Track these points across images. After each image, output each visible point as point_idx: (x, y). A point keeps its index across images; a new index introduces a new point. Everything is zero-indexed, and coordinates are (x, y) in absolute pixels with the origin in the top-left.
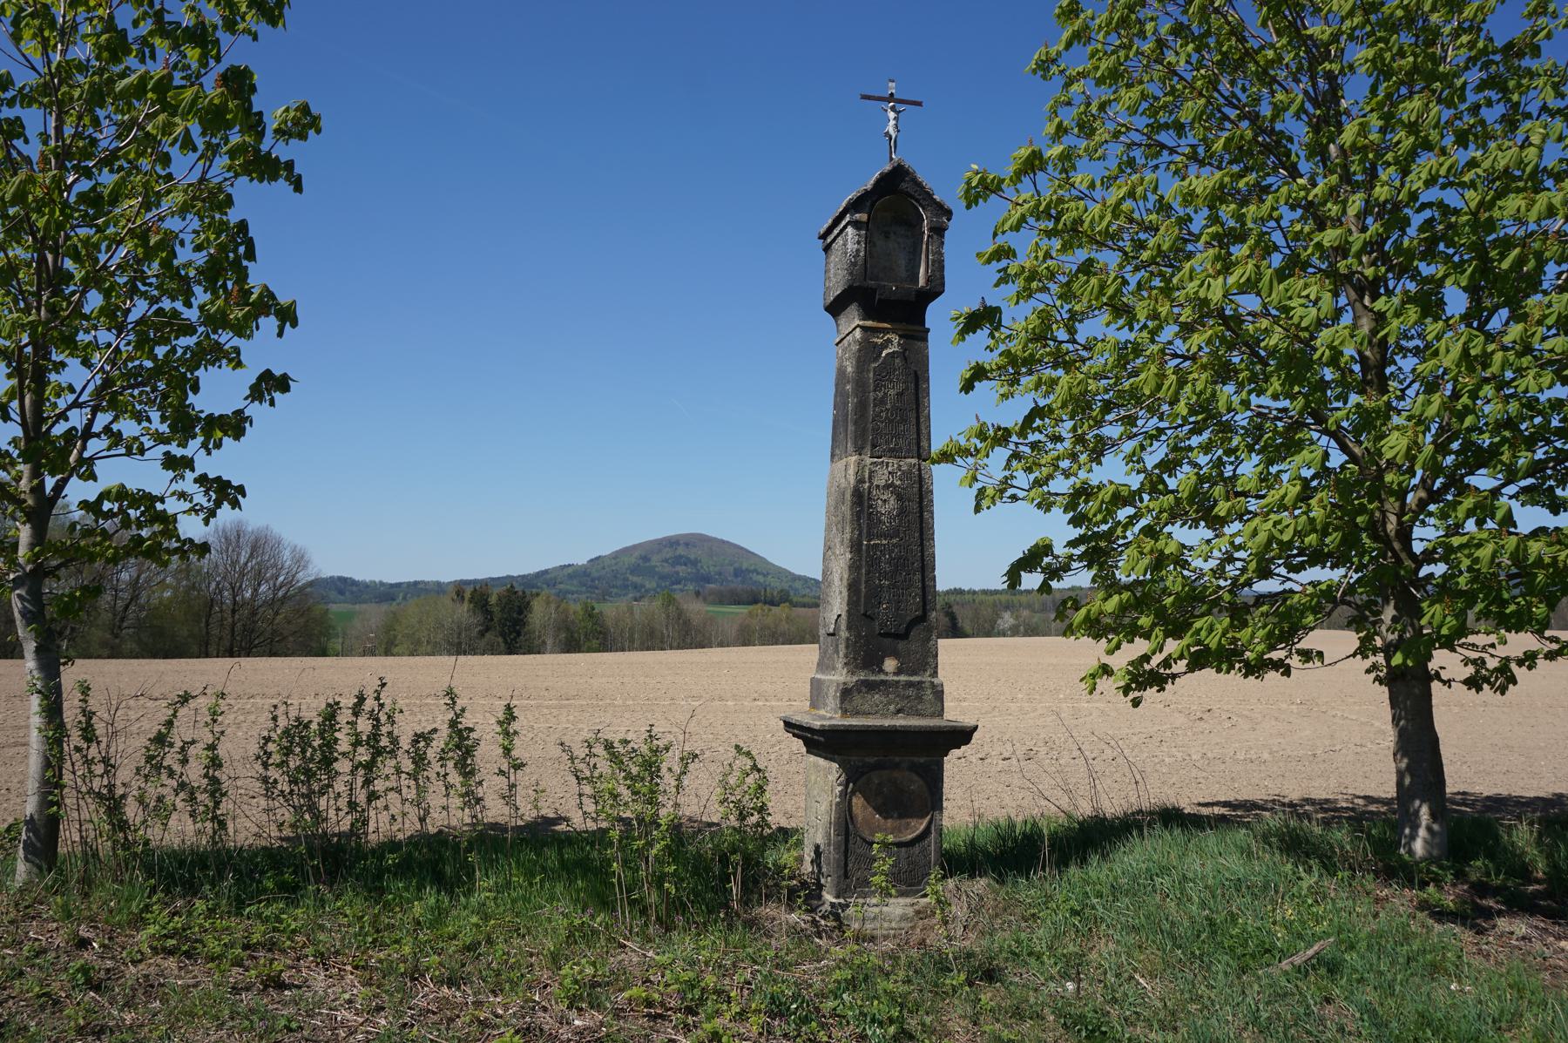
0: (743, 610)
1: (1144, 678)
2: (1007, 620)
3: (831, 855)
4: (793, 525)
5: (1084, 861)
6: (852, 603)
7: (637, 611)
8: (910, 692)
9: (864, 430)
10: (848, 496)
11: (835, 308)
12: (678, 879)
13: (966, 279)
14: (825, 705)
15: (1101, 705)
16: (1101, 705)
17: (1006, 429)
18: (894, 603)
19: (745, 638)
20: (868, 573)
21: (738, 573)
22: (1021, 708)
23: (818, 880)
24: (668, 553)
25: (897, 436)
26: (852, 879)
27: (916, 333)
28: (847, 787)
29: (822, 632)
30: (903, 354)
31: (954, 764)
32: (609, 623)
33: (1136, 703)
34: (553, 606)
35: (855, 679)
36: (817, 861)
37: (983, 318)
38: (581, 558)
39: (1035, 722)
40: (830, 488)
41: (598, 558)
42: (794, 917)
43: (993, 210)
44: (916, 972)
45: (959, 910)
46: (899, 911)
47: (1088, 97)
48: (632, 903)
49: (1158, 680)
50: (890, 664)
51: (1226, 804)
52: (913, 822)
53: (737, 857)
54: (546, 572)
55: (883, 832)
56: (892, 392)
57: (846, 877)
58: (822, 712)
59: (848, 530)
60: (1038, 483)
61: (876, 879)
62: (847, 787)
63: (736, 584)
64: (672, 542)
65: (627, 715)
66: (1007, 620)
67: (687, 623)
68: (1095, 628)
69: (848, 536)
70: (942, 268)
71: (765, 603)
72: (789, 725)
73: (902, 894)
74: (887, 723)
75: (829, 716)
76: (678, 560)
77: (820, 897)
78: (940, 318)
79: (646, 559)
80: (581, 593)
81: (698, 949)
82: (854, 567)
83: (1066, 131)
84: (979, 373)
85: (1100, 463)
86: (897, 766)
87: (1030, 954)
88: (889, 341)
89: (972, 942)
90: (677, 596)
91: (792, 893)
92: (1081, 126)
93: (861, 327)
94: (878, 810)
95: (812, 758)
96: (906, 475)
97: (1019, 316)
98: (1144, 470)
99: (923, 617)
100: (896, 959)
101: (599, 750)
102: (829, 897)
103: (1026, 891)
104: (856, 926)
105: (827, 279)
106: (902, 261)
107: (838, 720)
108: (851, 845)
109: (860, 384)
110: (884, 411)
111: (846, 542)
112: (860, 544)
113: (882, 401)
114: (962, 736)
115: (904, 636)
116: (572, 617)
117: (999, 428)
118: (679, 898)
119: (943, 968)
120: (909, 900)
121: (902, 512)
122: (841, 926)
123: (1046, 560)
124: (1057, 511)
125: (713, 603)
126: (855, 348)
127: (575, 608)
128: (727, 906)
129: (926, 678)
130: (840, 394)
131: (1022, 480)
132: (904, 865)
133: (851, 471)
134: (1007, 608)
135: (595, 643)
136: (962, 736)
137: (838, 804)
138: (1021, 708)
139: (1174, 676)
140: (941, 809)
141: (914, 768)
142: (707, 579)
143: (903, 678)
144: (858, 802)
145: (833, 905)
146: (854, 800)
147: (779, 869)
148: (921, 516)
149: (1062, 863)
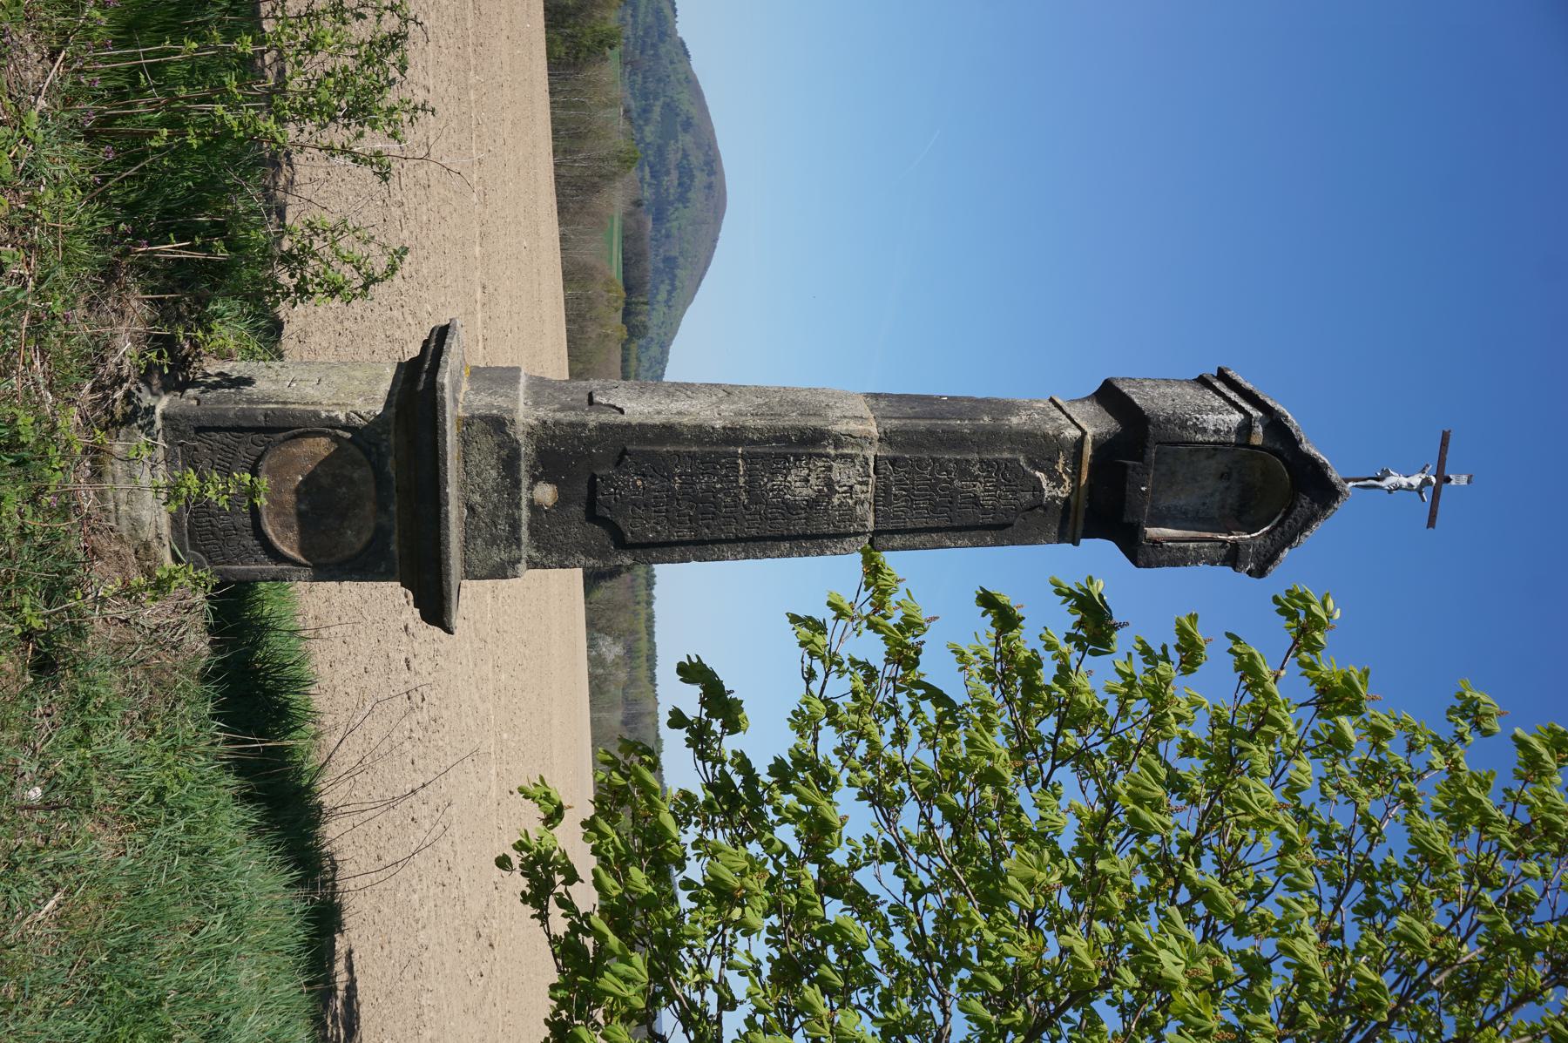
0: (616, 271)
1: (542, 876)
2: (612, 650)
3: (232, 404)
4: (754, 334)
5: (246, 798)
6: (642, 432)
8: (503, 527)
9: (919, 446)
10: (814, 422)
11: (1109, 396)
12: (179, 153)
13: (1147, 600)
14: (477, 392)
15: (494, 793)
16: (494, 793)
17: (916, 663)
18: (639, 497)
19: (574, 275)
20: (692, 456)
21: (671, 262)
22: (485, 680)
23: (194, 384)
24: (696, 159)
25: (910, 498)
26: (194, 439)
27: (1075, 523)
28: (345, 428)
29: (594, 384)
30: (1038, 505)
31: (390, 600)
32: (590, 72)
33: (503, 862)
35: (521, 438)
36: (227, 381)
37: (1094, 622)
38: (685, 27)
39: (460, 719)
40: (824, 392)
41: (686, 53)
42: (126, 346)
43: (1269, 642)
44: (42, 547)
45: (152, 612)
46: (146, 516)
47: (1420, 777)
48: (133, 73)
49: (538, 896)
50: (546, 493)
51: (351, 988)
52: (293, 536)
53: (222, 254)
55: (273, 489)
56: (979, 488)
57: (200, 430)
58: (465, 387)
59: (760, 423)
60: (832, 711)
61: (192, 479)
62: (345, 428)
63: (653, 261)
64: (712, 164)
65: (453, 90)
66: (612, 650)
67: (595, 188)
68: (610, 800)
69: (750, 422)
70: (1174, 563)
71: (627, 304)
72: (442, 333)
73: (175, 520)
74: (452, 490)
75: (459, 397)
76: (686, 173)
77: (166, 389)
78: (1097, 562)
79: (687, 125)
80: (635, 28)
81: (56, 184)
82: (701, 433)
83: (1376, 746)
84: (1006, 619)
85: (861, 798)
86: (382, 507)
87: (86, 728)
89: (100, 632)
90: (633, 173)
91: (169, 342)
92: (1378, 767)
93: (1080, 442)
94: (310, 479)
95: (390, 372)
96: (848, 514)
97: (1096, 679)
98: (854, 867)
99: (621, 544)
100: (64, 511)
101: (391, 23)
102: (162, 404)
103: (194, 717)
104: (118, 448)
105: (1157, 383)
106: (1184, 499)
108: (250, 436)
109: (993, 437)
110: (948, 477)
111: (741, 421)
112: (737, 442)
113: (964, 473)
114: (435, 609)
115: (592, 516)
116: (598, 14)
117: (918, 652)
118: (144, 155)
119: (53, 592)
120: (166, 531)
121: (790, 508)
122: (112, 425)
123: (716, 725)
124: (792, 738)
125: (624, 228)
126: (1049, 429)
128: (137, 235)
129: (526, 551)
130: (976, 406)
131: (839, 688)
132: (223, 522)
133: (853, 426)
134: (631, 652)
135: (561, 50)
136: (435, 609)
137: (316, 414)
138: (485, 680)
139: (543, 917)
140: (316, 579)
141: (381, 533)
142: (659, 218)
143: (525, 514)
144: (321, 447)
145: (150, 410)
146: (324, 441)
147: (204, 323)
148: (783, 538)
149: (241, 767)
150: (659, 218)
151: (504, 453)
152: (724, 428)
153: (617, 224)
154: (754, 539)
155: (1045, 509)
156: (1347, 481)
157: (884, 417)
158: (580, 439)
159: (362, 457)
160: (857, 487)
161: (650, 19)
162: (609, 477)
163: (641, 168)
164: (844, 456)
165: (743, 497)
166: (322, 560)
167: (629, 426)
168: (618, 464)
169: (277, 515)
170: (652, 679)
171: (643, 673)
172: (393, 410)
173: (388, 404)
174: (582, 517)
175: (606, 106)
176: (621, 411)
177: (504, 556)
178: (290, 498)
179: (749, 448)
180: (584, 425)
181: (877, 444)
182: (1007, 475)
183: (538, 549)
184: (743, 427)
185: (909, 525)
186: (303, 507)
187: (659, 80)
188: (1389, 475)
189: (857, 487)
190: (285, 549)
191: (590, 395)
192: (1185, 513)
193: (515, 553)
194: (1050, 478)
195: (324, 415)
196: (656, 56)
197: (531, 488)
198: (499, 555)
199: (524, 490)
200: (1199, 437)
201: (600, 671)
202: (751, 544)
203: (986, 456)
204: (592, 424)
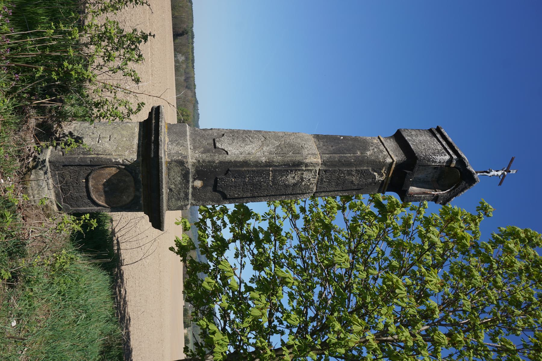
8: (182, 195)
9: (335, 166)
20: (252, 171)
25: (329, 182)
28: (122, 165)
31: (140, 220)
33: (171, 249)
35: (190, 167)
50: (198, 184)
56: (354, 178)
57: (64, 166)
62: (122, 165)
66: (181, 58)
82: (257, 164)
86: (137, 190)
88: (382, 175)
93: (392, 163)
94: (108, 181)
95: (137, 130)
96: (307, 187)
107: (164, 158)
112: (270, 166)
113: (350, 173)
115: (215, 189)
121: (287, 186)
134: (187, 59)
143: (190, 190)
146: (114, 169)
148: (283, 195)
151: (183, 172)
155: (375, 183)
156: (477, 173)
157: (323, 154)
158: (212, 166)
159: (129, 173)
160: (312, 179)
162: (222, 178)
166: (114, 206)
168: (226, 174)
169: (97, 192)
170: (193, 67)
171: (190, 65)
172: (141, 158)
173: (138, 156)
177: (182, 203)
178: (101, 187)
179: (274, 168)
182: (364, 174)
183: (195, 200)
186: (106, 189)
188: (492, 171)
189: (312, 179)
190: (100, 203)
192: (420, 179)
193: (187, 202)
194: (379, 174)
195: (114, 160)
197: (193, 182)
198: (180, 203)
199: (190, 183)
201: (178, 64)
203: (358, 168)
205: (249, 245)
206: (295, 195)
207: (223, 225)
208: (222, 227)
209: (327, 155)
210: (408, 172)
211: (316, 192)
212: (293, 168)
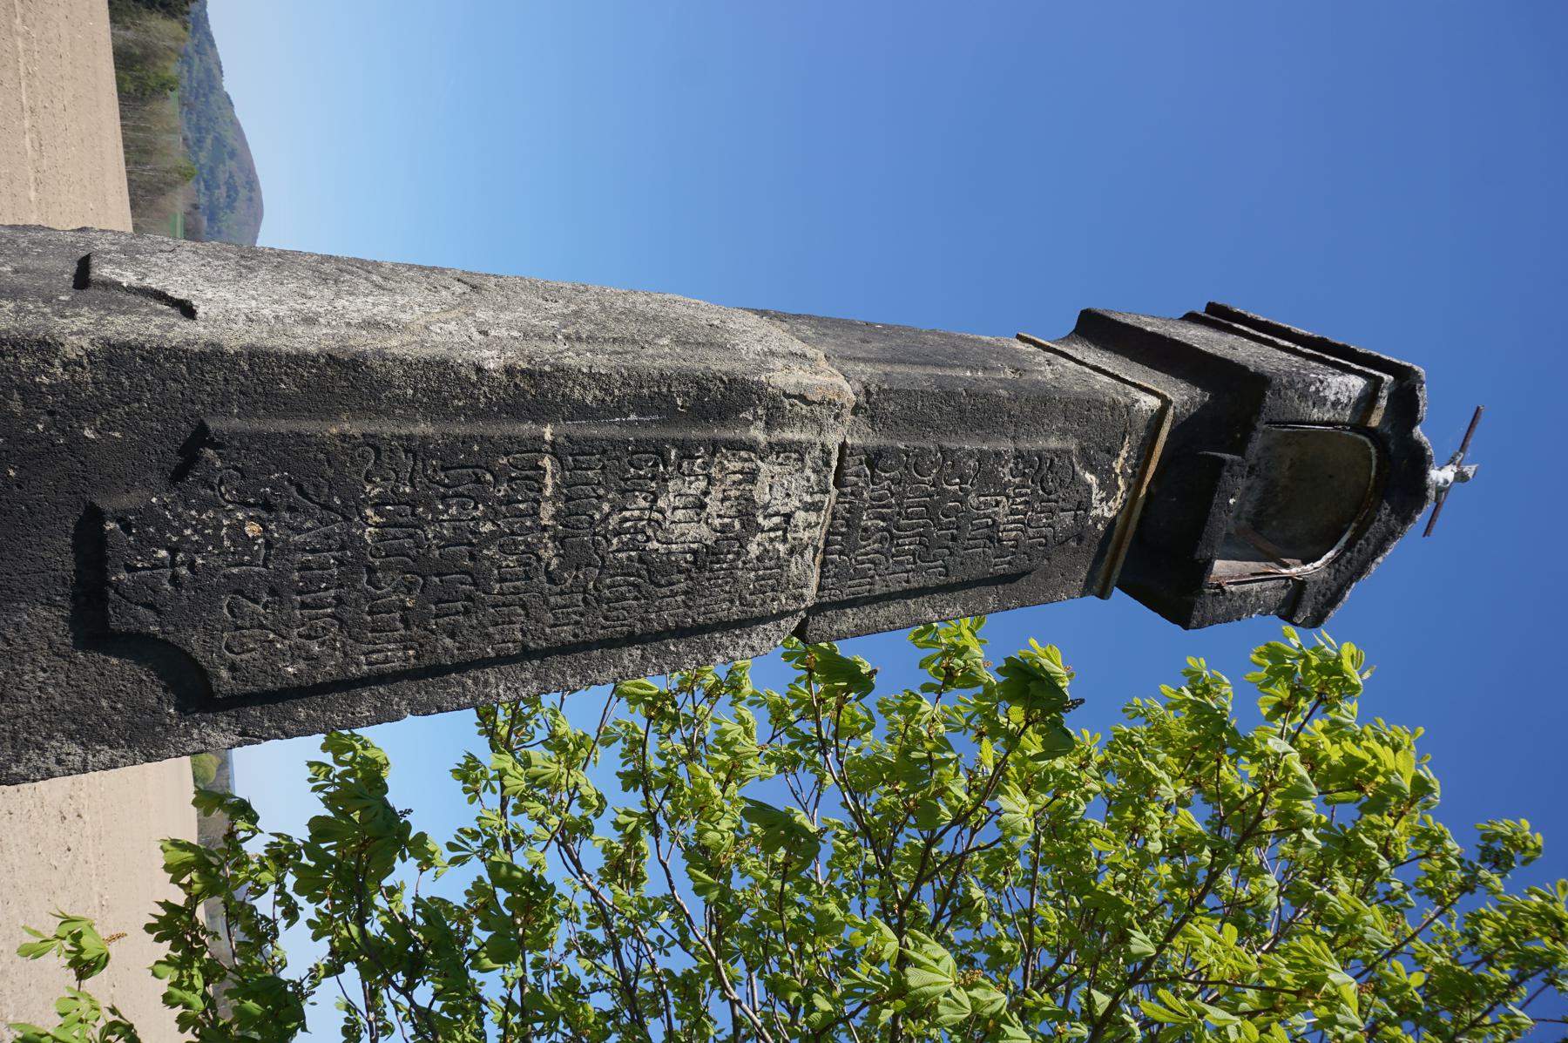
6: (261, 374)
7: (171, 138)
10: (718, 364)
20: (416, 449)
24: (240, 179)
32: (155, 106)
34: (172, 44)
41: (231, 103)
54: (213, 45)
59: (602, 362)
64: (252, 183)
67: (161, 192)
76: (232, 189)
79: (232, 155)
80: (190, 79)
82: (441, 383)
90: (191, 184)
96: (774, 573)
111: (549, 352)
112: (540, 411)
116: (159, 64)
121: (654, 571)
127: (173, 69)
148: (631, 640)
150: (212, 218)
152: (509, 371)
153: (179, 220)
154: (564, 649)
158: (30, 393)
160: (800, 516)
161: (202, 75)
162: (148, 515)
163: (198, 182)
164: (783, 448)
165: (549, 553)
167: (213, 355)
168: (178, 476)
174: (63, 637)
175: (168, 132)
176: (187, 310)
179: (569, 428)
180: (46, 347)
181: (849, 417)
184: (563, 371)
185: (879, 589)
187: (210, 120)
189: (800, 516)
191: (84, 265)
194: (1101, 486)
196: (207, 102)
200: (1316, 414)
202: (555, 660)
203: (1025, 445)
204: (75, 345)
205: (406, 991)
206: (697, 632)
207: (284, 914)
208: (282, 923)
209: (869, 369)
210: (1227, 456)
211: (818, 609)
212: (695, 434)
